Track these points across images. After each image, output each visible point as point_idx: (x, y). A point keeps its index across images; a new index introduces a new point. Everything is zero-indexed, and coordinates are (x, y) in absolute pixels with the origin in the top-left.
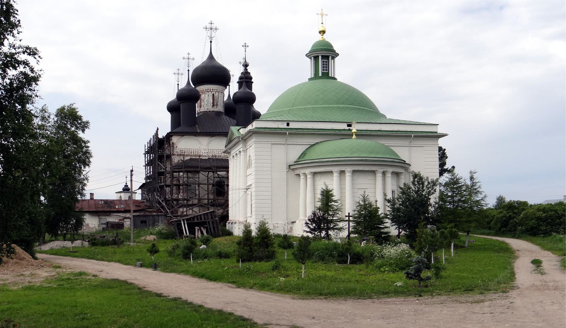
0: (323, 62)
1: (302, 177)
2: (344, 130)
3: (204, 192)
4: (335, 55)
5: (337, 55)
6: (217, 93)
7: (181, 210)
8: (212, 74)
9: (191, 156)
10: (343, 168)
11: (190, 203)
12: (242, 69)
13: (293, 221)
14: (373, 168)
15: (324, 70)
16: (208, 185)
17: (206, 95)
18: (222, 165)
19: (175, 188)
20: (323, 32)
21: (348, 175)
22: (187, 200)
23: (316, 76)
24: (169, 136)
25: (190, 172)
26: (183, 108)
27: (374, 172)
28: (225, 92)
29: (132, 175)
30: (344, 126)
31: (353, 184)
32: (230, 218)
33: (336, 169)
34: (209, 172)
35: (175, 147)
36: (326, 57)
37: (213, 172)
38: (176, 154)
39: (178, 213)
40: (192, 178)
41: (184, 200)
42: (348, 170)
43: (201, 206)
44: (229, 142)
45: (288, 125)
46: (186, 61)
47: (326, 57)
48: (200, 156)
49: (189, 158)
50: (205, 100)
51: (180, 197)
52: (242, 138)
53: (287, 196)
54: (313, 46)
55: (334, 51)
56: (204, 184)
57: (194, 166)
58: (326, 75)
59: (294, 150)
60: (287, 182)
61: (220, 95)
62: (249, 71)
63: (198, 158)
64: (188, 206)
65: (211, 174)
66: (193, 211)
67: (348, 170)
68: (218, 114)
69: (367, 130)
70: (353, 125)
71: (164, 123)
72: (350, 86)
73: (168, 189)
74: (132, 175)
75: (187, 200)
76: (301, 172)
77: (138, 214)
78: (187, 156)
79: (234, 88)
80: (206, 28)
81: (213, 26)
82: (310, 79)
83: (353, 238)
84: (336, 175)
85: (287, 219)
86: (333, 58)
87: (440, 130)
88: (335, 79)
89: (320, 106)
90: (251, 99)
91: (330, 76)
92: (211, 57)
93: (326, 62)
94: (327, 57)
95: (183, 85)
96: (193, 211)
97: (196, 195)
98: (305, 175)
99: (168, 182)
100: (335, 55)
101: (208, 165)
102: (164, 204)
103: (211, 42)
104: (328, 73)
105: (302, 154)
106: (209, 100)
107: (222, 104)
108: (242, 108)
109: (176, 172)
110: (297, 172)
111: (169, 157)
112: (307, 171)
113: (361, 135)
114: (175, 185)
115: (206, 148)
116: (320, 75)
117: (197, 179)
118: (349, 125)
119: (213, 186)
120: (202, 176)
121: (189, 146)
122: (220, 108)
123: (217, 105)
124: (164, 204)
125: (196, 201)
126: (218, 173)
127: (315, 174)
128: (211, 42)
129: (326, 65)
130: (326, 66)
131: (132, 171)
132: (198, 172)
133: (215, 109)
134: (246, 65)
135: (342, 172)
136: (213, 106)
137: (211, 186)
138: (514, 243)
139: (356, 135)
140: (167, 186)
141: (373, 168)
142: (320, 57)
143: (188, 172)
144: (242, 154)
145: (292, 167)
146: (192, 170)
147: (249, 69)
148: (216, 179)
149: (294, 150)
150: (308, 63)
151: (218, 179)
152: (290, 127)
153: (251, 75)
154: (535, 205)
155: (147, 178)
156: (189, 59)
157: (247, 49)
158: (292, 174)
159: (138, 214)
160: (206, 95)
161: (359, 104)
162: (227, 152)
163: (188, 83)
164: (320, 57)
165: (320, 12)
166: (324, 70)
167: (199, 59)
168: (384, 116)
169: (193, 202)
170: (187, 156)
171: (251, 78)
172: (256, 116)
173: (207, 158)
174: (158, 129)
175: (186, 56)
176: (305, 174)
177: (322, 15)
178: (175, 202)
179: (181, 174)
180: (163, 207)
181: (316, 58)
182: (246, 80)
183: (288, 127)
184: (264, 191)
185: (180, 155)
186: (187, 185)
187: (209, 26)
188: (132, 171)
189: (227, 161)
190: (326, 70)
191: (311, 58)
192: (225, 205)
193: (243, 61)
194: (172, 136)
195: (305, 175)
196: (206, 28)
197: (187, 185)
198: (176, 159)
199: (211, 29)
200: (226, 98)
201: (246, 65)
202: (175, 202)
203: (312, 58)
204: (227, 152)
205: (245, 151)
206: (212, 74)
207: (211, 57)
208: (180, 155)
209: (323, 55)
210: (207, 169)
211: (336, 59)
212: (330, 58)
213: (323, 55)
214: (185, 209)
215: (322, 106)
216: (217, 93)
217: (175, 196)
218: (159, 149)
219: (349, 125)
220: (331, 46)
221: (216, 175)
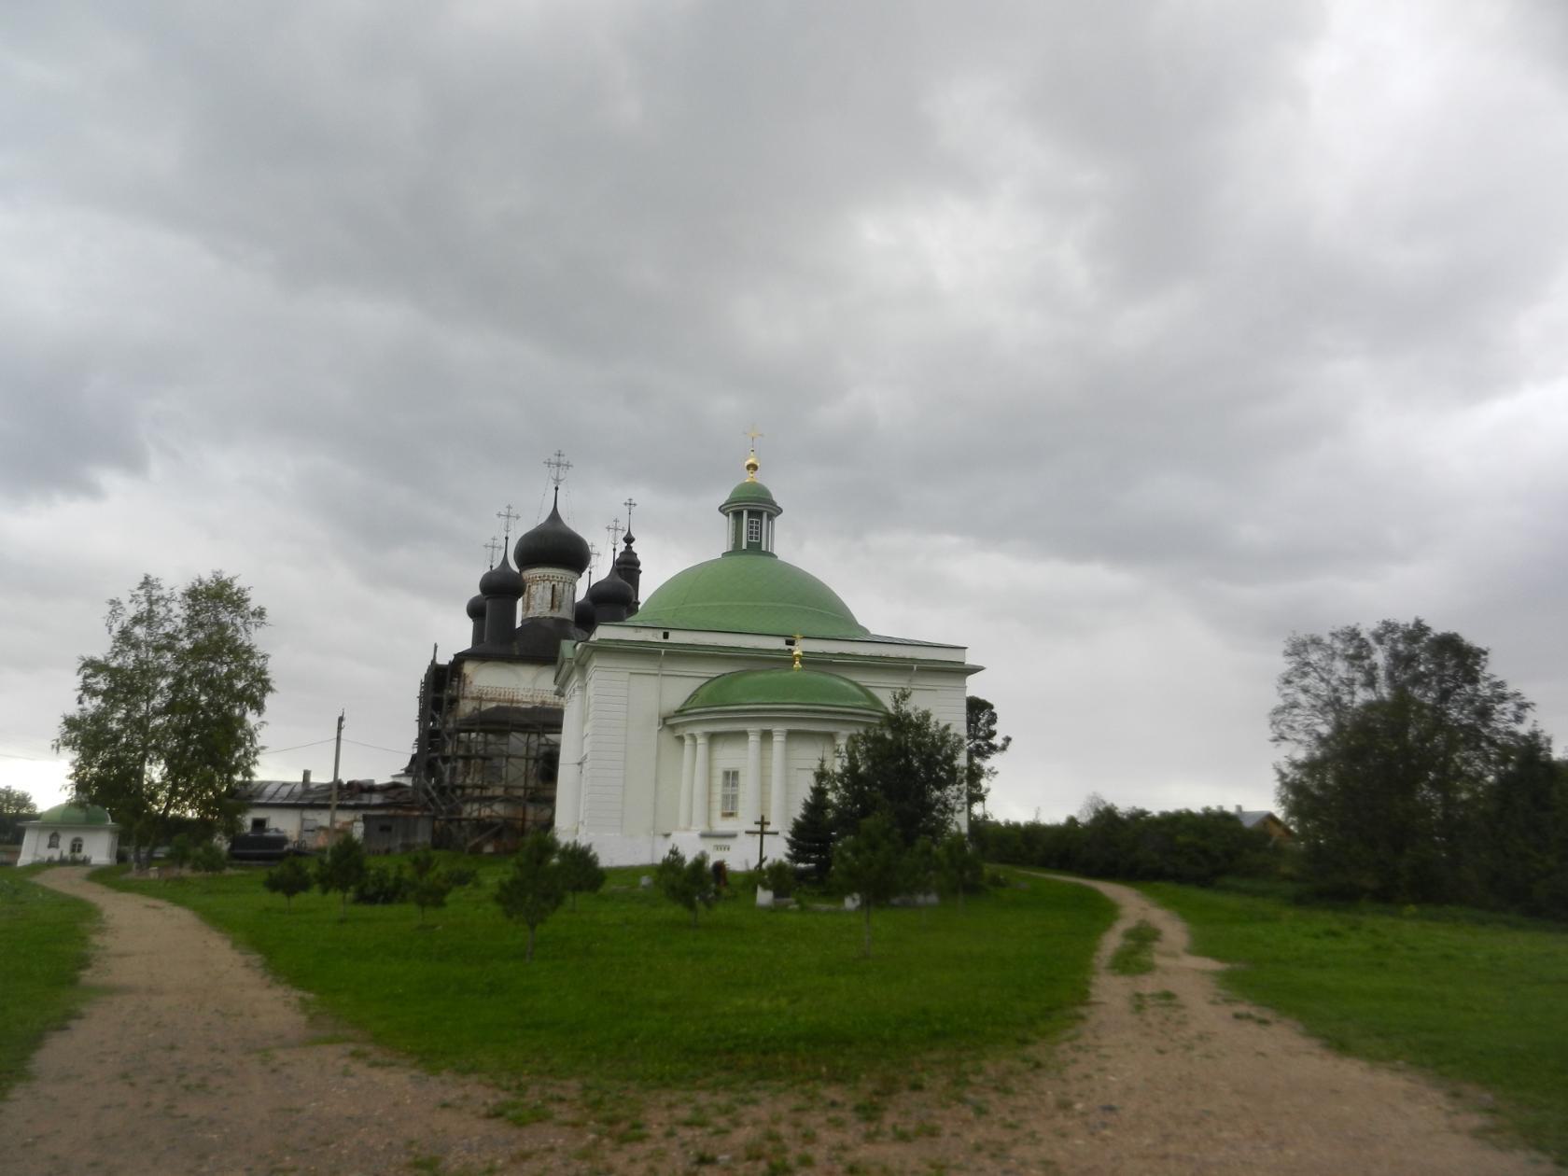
1: (688, 742)
3: (517, 772)
4: (775, 511)
5: (780, 511)
8: (555, 548)
10: (767, 726)
11: (489, 793)
12: (622, 547)
14: (830, 728)
18: (548, 720)
19: (460, 764)
20: (753, 467)
21: (778, 740)
22: (482, 788)
23: (736, 549)
24: (460, 658)
27: (831, 737)
29: (340, 728)
30: (779, 644)
31: (787, 758)
33: (754, 729)
41: (475, 787)
42: (779, 730)
43: (507, 800)
45: (666, 636)
49: (494, 705)
51: (468, 781)
53: (657, 781)
54: (735, 491)
55: (773, 503)
57: (503, 720)
58: (755, 548)
59: (678, 687)
64: (483, 800)
65: (534, 737)
67: (779, 730)
68: (561, 622)
71: (457, 634)
74: (340, 728)
76: (689, 730)
77: (392, 812)
78: (492, 700)
84: (754, 739)
86: (770, 517)
92: (555, 516)
98: (693, 737)
100: (775, 511)
101: (527, 721)
110: (679, 732)
111: (454, 701)
112: (698, 730)
113: (811, 661)
118: (790, 643)
119: (536, 760)
120: (517, 741)
122: (566, 613)
125: (499, 791)
130: (756, 532)
131: (341, 719)
133: (557, 614)
134: (629, 540)
135: (766, 736)
138: (1108, 889)
141: (830, 728)
143: (486, 732)
145: (670, 722)
148: (544, 749)
149: (678, 687)
150: (724, 525)
158: (667, 736)
159: (392, 812)
162: (560, 693)
167: (531, 520)
168: (866, 631)
170: (492, 700)
171: (638, 564)
175: (513, 512)
180: (432, 800)
181: (738, 515)
188: (341, 719)
192: (551, 801)
195: (693, 737)
198: (466, 707)
201: (629, 540)
204: (560, 693)
205: (583, 688)
207: (555, 516)
210: (524, 728)
214: (476, 806)
217: (459, 781)
218: (441, 684)
219: (790, 643)
221: (543, 740)
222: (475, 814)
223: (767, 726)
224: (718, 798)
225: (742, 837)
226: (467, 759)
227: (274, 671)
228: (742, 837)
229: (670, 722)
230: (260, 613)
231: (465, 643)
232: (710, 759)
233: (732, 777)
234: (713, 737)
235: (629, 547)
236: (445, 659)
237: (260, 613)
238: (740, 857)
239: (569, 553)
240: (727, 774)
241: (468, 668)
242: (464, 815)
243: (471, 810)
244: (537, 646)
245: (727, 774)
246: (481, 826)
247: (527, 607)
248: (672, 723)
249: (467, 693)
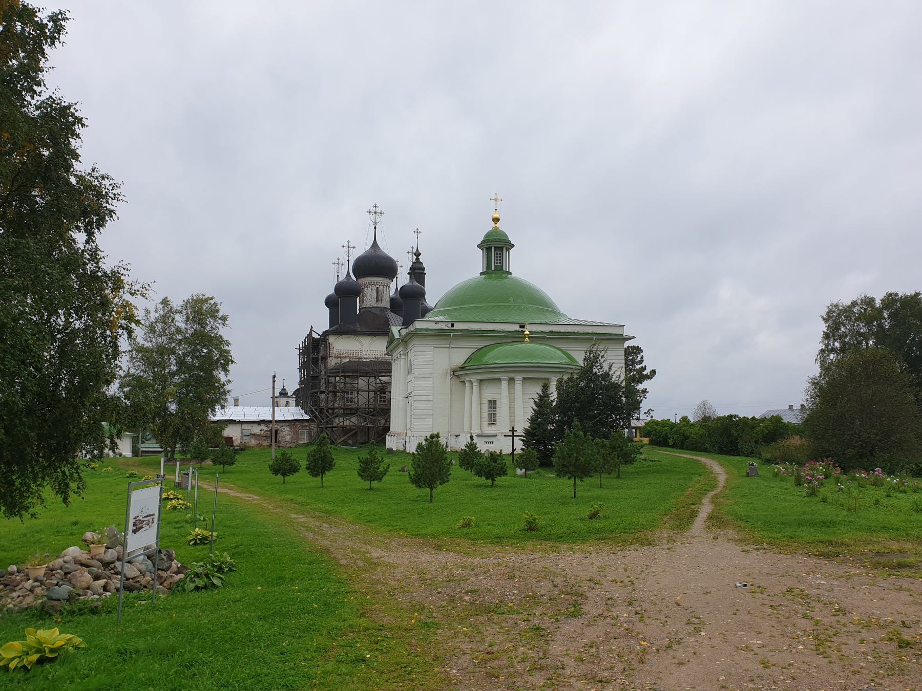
7: (337, 420)
8: (375, 265)
10: (511, 375)
16: (369, 391)
18: (382, 368)
19: (330, 395)
21: (518, 384)
23: (487, 272)
24: (326, 334)
25: (349, 377)
26: (342, 301)
29: (274, 382)
30: (516, 328)
33: (505, 377)
36: (499, 249)
42: (518, 377)
44: (389, 344)
45: (453, 325)
55: (509, 242)
57: (356, 369)
65: (372, 379)
71: (321, 322)
73: (322, 396)
74: (274, 382)
79: (403, 278)
81: (378, 210)
82: (481, 274)
84: (505, 383)
86: (508, 250)
87: (626, 333)
90: (421, 294)
95: (342, 277)
99: (322, 389)
106: (377, 294)
107: (388, 300)
108: (410, 302)
110: (462, 378)
111: (325, 359)
112: (473, 378)
116: (493, 268)
117: (356, 386)
120: (362, 382)
121: (346, 348)
122: (386, 304)
127: (481, 381)
130: (500, 259)
131: (274, 377)
132: (357, 377)
135: (511, 380)
137: (372, 394)
138: (703, 459)
140: (322, 392)
142: (493, 249)
143: (345, 377)
145: (457, 373)
149: (459, 355)
152: (455, 328)
154: (763, 420)
155: (301, 383)
161: (537, 302)
164: (493, 249)
165: (494, 197)
167: (361, 248)
170: (345, 358)
171: (424, 269)
172: (426, 311)
175: (346, 244)
177: (496, 200)
178: (330, 411)
179: (338, 379)
181: (488, 250)
182: (417, 272)
184: (427, 401)
185: (338, 357)
188: (274, 377)
189: (390, 364)
193: (415, 250)
198: (332, 362)
199: (375, 213)
200: (392, 292)
202: (330, 411)
205: (406, 354)
206: (375, 265)
208: (338, 357)
209: (496, 246)
210: (366, 374)
213: (496, 246)
214: (341, 419)
217: (330, 406)
218: (314, 350)
223: (511, 375)
224: (485, 415)
225: (500, 438)
226: (334, 393)
227: (234, 351)
228: (500, 438)
229: (457, 373)
230: (224, 319)
231: (326, 326)
233: (493, 404)
234: (481, 381)
237: (224, 319)
238: (503, 445)
239: (386, 268)
240: (490, 401)
241: (331, 339)
242: (335, 425)
243: (338, 421)
244: (375, 325)
245: (490, 401)
246: (345, 430)
247: (361, 302)
248: (459, 373)
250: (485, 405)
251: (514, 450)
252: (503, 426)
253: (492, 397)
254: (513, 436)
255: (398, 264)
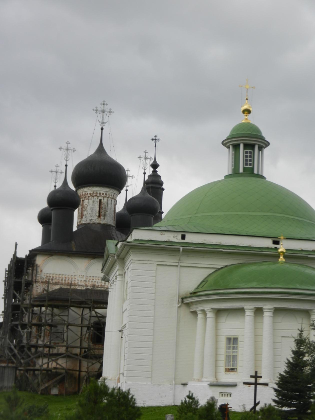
0: (247, 152)
1: (200, 316)
2: (268, 248)
3: (75, 336)
5: (267, 144)
6: (106, 199)
7: (40, 362)
8: (101, 173)
9: (62, 284)
10: (259, 305)
11: (55, 351)
13: (184, 382)
15: (246, 164)
17: (91, 201)
18: (99, 298)
19: (34, 329)
20: (248, 111)
21: (267, 314)
22: (50, 347)
23: (235, 173)
24: (34, 253)
25: (57, 307)
28: (118, 199)
30: (268, 243)
31: (274, 329)
32: (103, 375)
33: (249, 306)
34: (84, 308)
35: (39, 270)
37: (90, 308)
38: (40, 280)
39: (35, 365)
40: (59, 316)
41: (45, 346)
42: (268, 307)
43: (68, 356)
45: (183, 237)
46: (64, 152)
47: (249, 146)
48: (71, 285)
49: (58, 287)
50: (89, 209)
51: (40, 342)
52: (118, 256)
54: (234, 130)
55: (263, 138)
56: (77, 326)
57: (63, 298)
58: (249, 172)
60: (178, 322)
61: (109, 202)
62: (159, 173)
63: (68, 287)
64: (50, 356)
65: (87, 311)
66: (57, 364)
68: (106, 227)
69: (302, 250)
70: (281, 243)
72: (282, 188)
75: (50, 347)
76: (199, 308)
78: (56, 284)
80: (97, 110)
82: (226, 177)
83: (296, 417)
84: (249, 314)
85: (175, 379)
86: (261, 149)
88: (262, 177)
89: (236, 213)
91: (256, 172)
93: (250, 153)
94: (252, 146)
96: (57, 364)
97: (64, 341)
101: (81, 299)
102: (16, 351)
103: (102, 129)
104: (253, 169)
105: (203, 282)
107: (112, 214)
109: (37, 306)
110: (194, 308)
111: (29, 284)
112: (208, 307)
113: (291, 256)
114: (35, 325)
115: (84, 274)
116: (241, 170)
117: (65, 318)
118: (276, 242)
119: (88, 328)
120: (74, 313)
121: (60, 271)
122: (109, 220)
123: (105, 215)
124: (16, 351)
125: (62, 350)
126: (97, 310)
128: (102, 129)
129: (250, 157)
130: (250, 159)
133: (103, 221)
134: (155, 166)
135: (259, 311)
136: (99, 216)
137: (85, 329)
139: (285, 257)
142: (242, 146)
143: (53, 307)
144: (118, 279)
145: (186, 301)
146: (60, 303)
147: (159, 171)
148: (94, 320)
149: (193, 275)
151: (96, 319)
153: (163, 179)
156: (67, 150)
157: (158, 143)
158: (185, 311)
160: (91, 201)
162: (106, 279)
163: (65, 183)
164: (242, 146)
166: (246, 164)
167: (85, 152)
169: (58, 350)
170: (56, 284)
171: (162, 184)
173: (83, 288)
174: (16, 245)
176: (204, 311)
178: (33, 350)
179: (43, 309)
180: (14, 355)
181: (236, 147)
183: (183, 241)
186: (51, 326)
187: (154, 138)
189: (106, 293)
190: (250, 164)
191: (228, 147)
192: (100, 358)
194: (35, 255)
196: (97, 110)
197: (51, 326)
199: (103, 111)
201: (155, 166)
202: (33, 350)
203: (231, 147)
204: (106, 279)
205: (123, 275)
209: (247, 144)
210: (80, 304)
211: (266, 151)
212: (256, 148)
214: (45, 360)
215: (239, 213)
216: (106, 199)
217: (33, 342)
219: (276, 242)
220: (258, 131)
221: (93, 313)
222: (45, 366)
224: (222, 358)
226: (39, 326)
229: (186, 301)
232: (216, 328)
233: (233, 342)
234: (218, 312)
235: (155, 172)
236: (22, 254)
240: (229, 339)
241: (39, 260)
242: (37, 367)
243: (43, 363)
244: (90, 244)
245: (229, 339)
246: (50, 374)
247: (81, 216)
248: (188, 301)
249: (39, 278)
250: (223, 344)
251: (256, 404)
252: (243, 374)
253: (232, 334)
254: (256, 384)
255: (128, 174)
